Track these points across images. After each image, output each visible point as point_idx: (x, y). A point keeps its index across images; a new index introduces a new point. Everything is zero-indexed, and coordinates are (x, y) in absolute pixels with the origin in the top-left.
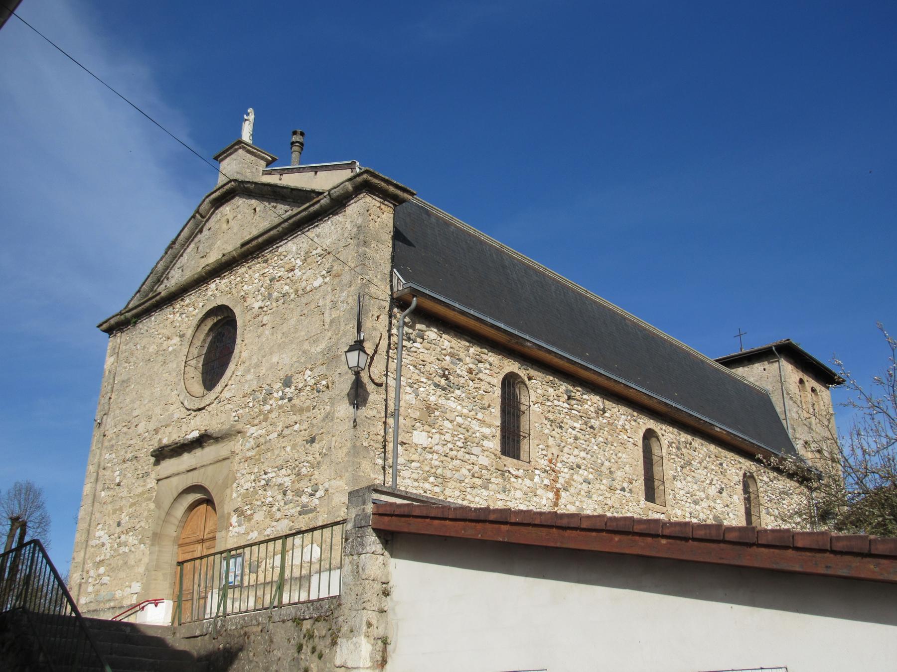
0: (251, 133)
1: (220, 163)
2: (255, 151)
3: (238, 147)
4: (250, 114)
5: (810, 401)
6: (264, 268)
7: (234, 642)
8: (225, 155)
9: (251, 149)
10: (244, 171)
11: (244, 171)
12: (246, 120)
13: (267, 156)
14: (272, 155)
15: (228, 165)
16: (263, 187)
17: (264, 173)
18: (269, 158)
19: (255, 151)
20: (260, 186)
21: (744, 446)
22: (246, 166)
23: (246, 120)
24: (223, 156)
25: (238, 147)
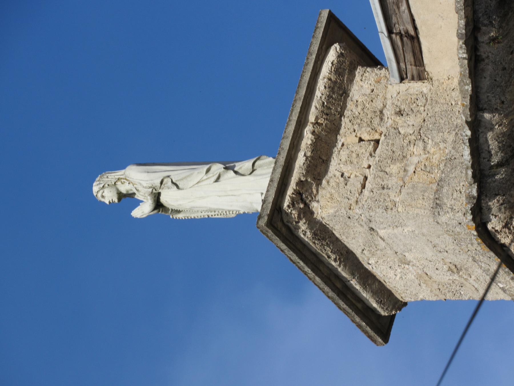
0: (217, 168)
1: (401, 305)
2: (308, 138)
3: (303, 226)
4: (124, 188)
5: (343, 206)
6: (399, 149)
7: (207, 175)
8: (354, 283)
9: (300, 160)
10: (422, 177)
11: (422, 177)
12: (158, 205)
13: (326, 69)
14: (315, 48)
15: (404, 262)
16: (489, 69)
17: (411, 69)
18: (332, 56)
19: (308, 138)
20: (485, 83)
21: (396, 46)
22: (394, 169)
23: (158, 205)
24: (365, 295)
25: (303, 226)
